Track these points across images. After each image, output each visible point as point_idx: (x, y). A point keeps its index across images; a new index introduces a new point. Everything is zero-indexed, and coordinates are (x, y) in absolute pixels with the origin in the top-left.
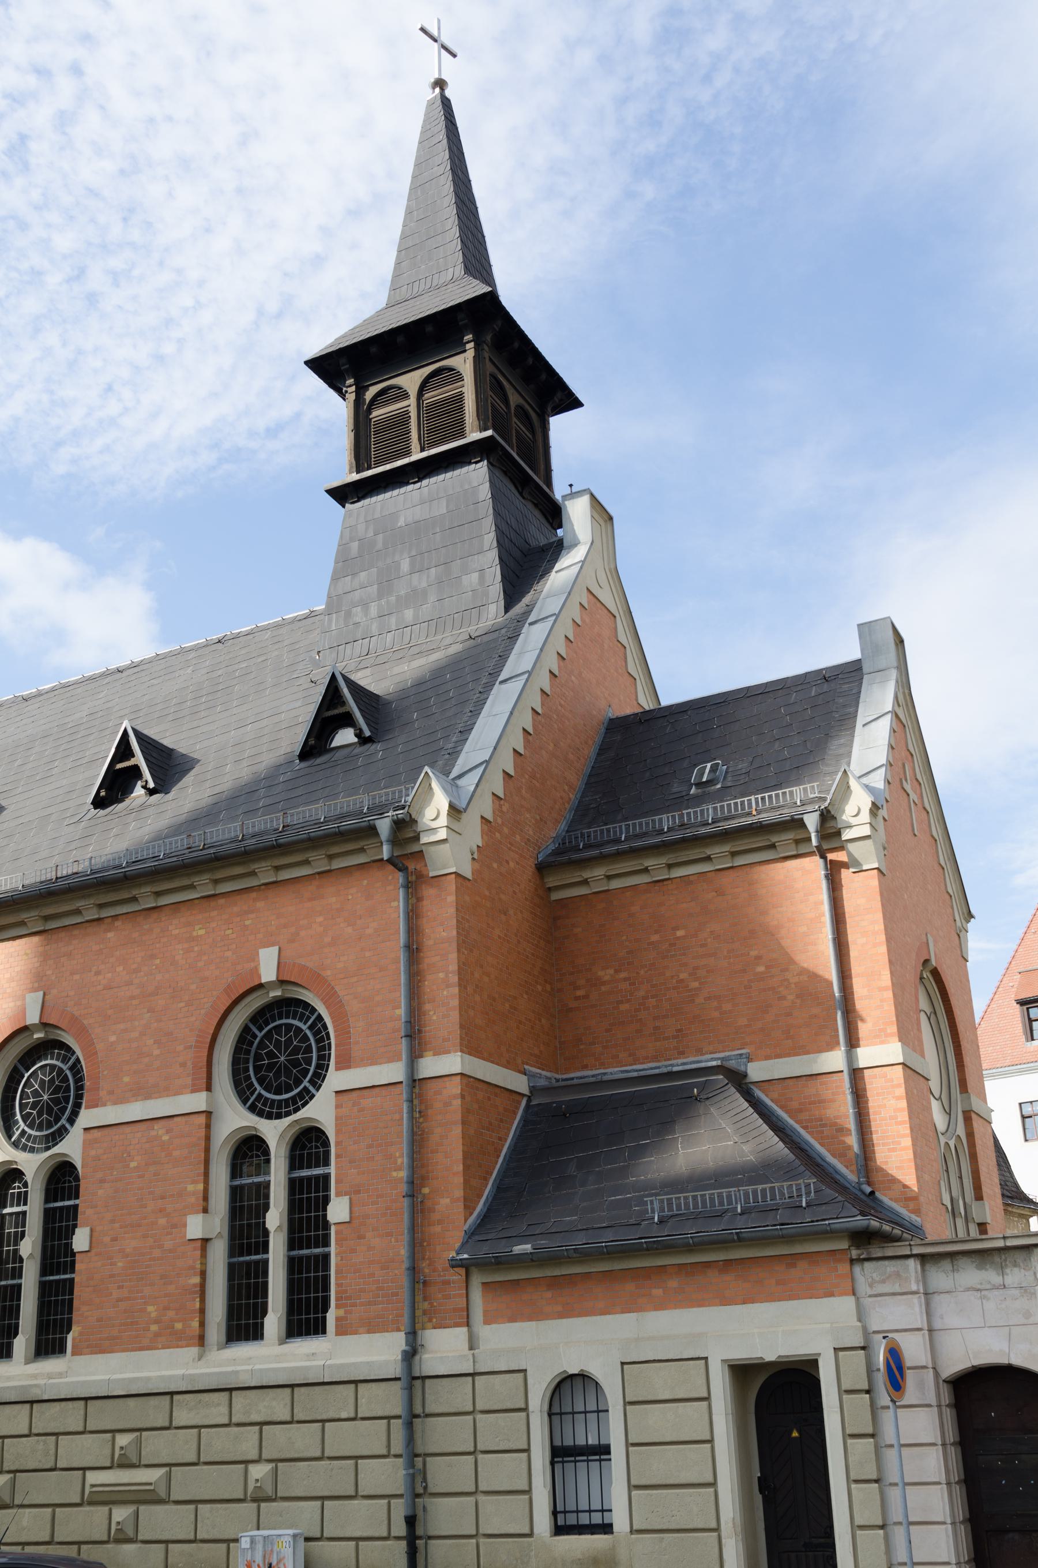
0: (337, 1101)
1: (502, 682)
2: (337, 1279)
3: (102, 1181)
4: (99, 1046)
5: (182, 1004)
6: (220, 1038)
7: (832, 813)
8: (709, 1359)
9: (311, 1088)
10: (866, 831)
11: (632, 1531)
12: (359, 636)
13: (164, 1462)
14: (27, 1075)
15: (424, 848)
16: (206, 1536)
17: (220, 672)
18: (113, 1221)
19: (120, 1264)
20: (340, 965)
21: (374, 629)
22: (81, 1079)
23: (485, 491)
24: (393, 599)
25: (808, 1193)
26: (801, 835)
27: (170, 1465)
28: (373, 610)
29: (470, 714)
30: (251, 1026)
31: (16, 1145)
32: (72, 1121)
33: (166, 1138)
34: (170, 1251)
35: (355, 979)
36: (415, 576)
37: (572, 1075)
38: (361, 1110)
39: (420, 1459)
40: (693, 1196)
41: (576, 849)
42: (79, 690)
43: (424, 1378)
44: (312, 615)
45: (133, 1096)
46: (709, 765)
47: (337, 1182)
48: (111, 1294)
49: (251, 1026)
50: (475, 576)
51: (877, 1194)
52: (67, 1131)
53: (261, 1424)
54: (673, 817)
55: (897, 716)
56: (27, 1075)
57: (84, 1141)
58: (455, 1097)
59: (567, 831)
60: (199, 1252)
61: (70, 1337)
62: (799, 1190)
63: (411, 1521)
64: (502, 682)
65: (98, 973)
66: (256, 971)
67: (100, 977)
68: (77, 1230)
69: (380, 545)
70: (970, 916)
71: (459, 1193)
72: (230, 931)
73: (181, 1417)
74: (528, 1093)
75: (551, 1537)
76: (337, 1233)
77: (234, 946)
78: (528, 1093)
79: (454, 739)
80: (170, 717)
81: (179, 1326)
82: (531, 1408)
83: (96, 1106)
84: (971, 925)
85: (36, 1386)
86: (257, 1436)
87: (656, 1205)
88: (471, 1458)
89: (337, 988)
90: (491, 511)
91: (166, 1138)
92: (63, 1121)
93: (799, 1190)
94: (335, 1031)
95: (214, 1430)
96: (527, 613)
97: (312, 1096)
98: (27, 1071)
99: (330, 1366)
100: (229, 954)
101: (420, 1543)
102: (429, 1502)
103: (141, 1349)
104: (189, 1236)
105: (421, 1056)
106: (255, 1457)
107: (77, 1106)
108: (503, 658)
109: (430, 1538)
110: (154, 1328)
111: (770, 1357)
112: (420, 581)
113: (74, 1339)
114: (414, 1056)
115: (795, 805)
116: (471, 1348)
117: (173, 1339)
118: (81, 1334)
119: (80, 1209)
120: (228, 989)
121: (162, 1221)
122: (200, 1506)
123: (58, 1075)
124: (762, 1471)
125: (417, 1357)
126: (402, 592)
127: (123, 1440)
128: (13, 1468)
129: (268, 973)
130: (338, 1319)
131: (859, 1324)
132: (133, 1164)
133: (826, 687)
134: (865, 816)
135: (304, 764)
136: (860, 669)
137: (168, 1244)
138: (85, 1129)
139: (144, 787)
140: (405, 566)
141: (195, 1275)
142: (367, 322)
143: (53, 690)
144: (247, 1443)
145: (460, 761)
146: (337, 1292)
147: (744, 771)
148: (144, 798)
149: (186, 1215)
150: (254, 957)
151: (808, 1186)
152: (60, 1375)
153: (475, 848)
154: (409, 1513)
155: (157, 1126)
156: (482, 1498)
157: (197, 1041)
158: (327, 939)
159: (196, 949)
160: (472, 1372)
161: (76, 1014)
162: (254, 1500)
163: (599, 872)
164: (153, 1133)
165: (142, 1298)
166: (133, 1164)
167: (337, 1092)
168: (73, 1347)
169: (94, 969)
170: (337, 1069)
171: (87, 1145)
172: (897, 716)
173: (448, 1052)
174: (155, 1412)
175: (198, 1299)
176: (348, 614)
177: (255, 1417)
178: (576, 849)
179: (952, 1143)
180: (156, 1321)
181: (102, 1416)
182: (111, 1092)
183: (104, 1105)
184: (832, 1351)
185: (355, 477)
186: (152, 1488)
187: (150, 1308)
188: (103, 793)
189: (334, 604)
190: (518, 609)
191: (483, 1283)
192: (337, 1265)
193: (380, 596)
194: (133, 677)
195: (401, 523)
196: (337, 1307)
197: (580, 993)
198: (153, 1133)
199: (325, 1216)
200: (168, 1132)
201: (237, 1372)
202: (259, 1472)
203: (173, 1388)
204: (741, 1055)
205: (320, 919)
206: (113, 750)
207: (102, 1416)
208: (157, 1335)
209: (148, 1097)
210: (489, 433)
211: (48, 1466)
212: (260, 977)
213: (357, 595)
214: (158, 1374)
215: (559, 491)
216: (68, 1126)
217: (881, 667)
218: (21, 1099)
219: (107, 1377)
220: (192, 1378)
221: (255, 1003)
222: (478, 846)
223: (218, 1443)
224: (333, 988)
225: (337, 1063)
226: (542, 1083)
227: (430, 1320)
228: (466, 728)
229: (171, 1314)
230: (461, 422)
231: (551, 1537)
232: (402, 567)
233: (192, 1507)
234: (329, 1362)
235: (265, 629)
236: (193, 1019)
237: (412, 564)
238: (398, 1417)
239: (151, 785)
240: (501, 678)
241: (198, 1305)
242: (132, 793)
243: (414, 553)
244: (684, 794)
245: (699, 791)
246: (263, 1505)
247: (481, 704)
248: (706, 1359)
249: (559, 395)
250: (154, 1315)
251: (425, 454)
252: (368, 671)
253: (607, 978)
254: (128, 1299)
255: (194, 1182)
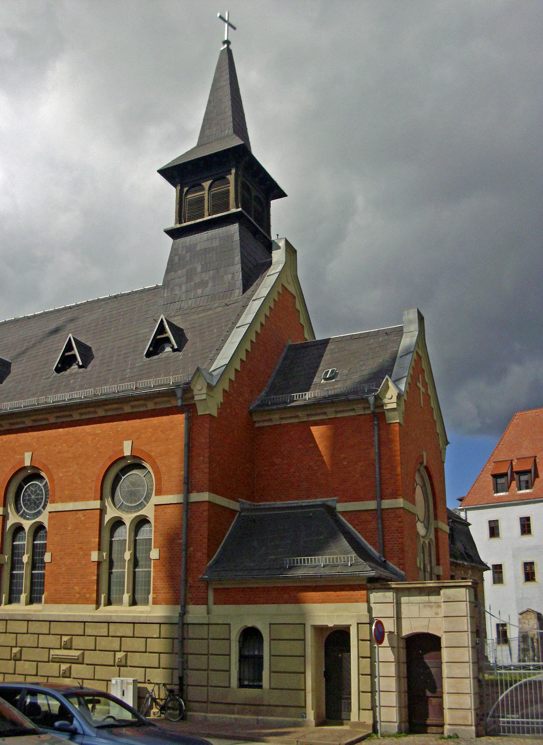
0: (155, 509)
1: (237, 328)
2: (153, 582)
3: (56, 534)
4: (55, 477)
5: (90, 462)
6: (107, 478)
7: (381, 397)
8: (306, 625)
9: (145, 502)
10: (394, 406)
11: (270, 688)
12: (177, 300)
13: (82, 648)
14: (25, 487)
15: (196, 402)
16: (98, 678)
17: (115, 312)
18: (60, 551)
19: (64, 569)
20: (158, 451)
21: (184, 298)
22: (48, 491)
23: (237, 237)
24: (193, 283)
25: (351, 560)
26: (367, 405)
27: (84, 650)
28: (184, 289)
29: (222, 341)
30: (120, 473)
31: (22, 516)
32: (44, 507)
33: (83, 518)
34: (85, 565)
35: (164, 457)
36: (203, 274)
37: (260, 503)
38: (165, 513)
39: (185, 655)
40: (307, 559)
41: (268, 405)
42: (52, 316)
43: (188, 624)
44: (157, 287)
45: (69, 500)
46: (330, 370)
47: (154, 542)
48: (60, 581)
49: (120, 473)
50: (230, 276)
51: (387, 562)
52: (42, 512)
53: (121, 637)
54: (311, 393)
55: (417, 353)
56: (25, 487)
57: (49, 518)
58: (205, 511)
59: (265, 396)
60: (96, 567)
61: (43, 596)
62: (348, 558)
63: (181, 679)
64: (237, 328)
65: (55, 446)
66: (122, 451)
67: (56, 448)
68: (46, 554)
69: (188, 259)
70: (447, 443)
71: (205, 551)
72: (111, 432)
73: (88, 631)
74: (240, 511)
75: (238, 688)
76: (154, 563)
77: (113, 439)
78: (240, 511)
79: (213, 353)
80: (91, 332)
81: (88, 595)
82: (232, 639)
83: (54, 503)
84: (448, 447)
85: (30, 614)
86: (119, 641)
87: (288, 561)
88: (206, 656)
89: (157, 461)
90: (239, 246)
91: (83, 518)
92: (40, 508)
93: (348, 558)
94: (155, 479)
95: (102, 638)
96: (252, 295)
97: (146, 506)
98: (26, 485)
99: (150, 616)
100: (111, 442)
101: (185, 687)
102: (189, 672)
103: (72, 603)
104: (92, 560)
105: (191, 492)
106: (119, 650)
107: (46, 502)
108: (239, 316)
109: (189, 685)
110: (78, 595)
111: (331, 625)
112: (206, 277)
113: (45, 598)
114: (188, 492)
115: (363, 392)
116: (208, 613)
117: (84, 600)
118: (48, 595)
119: (47, 545)
120: (110, 458)
121: (81, 553)
122: (96, 666)
123: (39, 488)
124: (325, 669)
125: (185, 616)
126: (197, 281)
127: (65, 639)
128: (21, 646)
129: (127, 452)
130: (153, 598)
131: (368, 614)
132: (69, 528)
133: (386, 337)
134: (394, 399)
135: (148, 359)
136: (402, 330)
137: (84, 562)
138: (49, 512)
139: (78, 364)
140: (199, 269)
141: (95, 575)
142: (169, 164)
143: (41, 314)
144: (115, 644)
145: (215, 364)
146: (153, 587)
147: (346, 374)
148: (77, 369)
149: (91, 551)
150: (121, 445)
151: (351, 557)
152: (39, 611)
153: (220, 403)
154: (181, 675)
155: (79, 513)
156: (211, 673)
157: (96, 479)
158: (153, 439)
159: (97, 439)
160: (208, 623)
161: (46, 463)
162: (118, 666)
163: (277, 416)
164: (77, 516)
165: (73, 583)
166: (69, 528)
167: (155, 505)
168: (45, 600)
169: (54, 444)
170: (156, 495)
171: (50, 519)
172: (417, 353)
173: (203, 491)
174: (78, 629)
175: (96, 586)
176: (172, 289)
177: (119, 634)
178: (268, 405)
179: (427, 542)
180: (79, 593)
181: (56, 629)
182: (60, 498)
183: (57, 502)
184: (356, 624)
185: (178, 226)
186: (77, 658)
187: (76, 588)
188: (60, 366)
189: (167, 283)
190: (249, 292)
191: (214, 589)
192: (153, 576)
193: (187, 283)
194: (76, 312)
195: (198, 248)
196: (153, 593)
197: (266, 468)
198: (77, 516)
199: (149, 556)
200: (84, 516)
201: (111, 616)
202: (119, 655)
203: (85, 620)
204: (334, 500)
205: (150, 430)
206: (64, 347)
207: (56, 629)
208: (79, 598)
209: (76, 500)
210: (240, 209)
211: (35, 646)
212: (124, 453)
213: (177, 281)
214: (79, 614)
215: (273, 237)
216: (42, 510)
217: (412, 330)
218: (23, 498)
219: (59, 613)
220: (94, 617)
221: (121, 465)
222: (221, 403)
223: (103, 643)
224: (155, 460)
225: (155, 493)
226: (247, 506)
227: (192, 601)
228: (220, 348)
229: (85, 591)
230: (228, 203)
231: (238, 688)
232: (197, 269)
233: (93, 666)
234: (149, 615)
235: (136, 292)
236: (95, 469)
237: (202, 268)
238: (177, 638)
239: (81, 364)
240: (238, 325)
241: (95, 588)
242: (72, 366)
243: (203, 263)
244: (318, 382)
245: (325, 381)
246: (121, 668)
247: (227, 337)
248: (304, 624)
249: (276, 191)
250: (78, 590)
251: (210, 217)
252: (179, 317)
253: (278, 463)
254: (67, 583)
255: (94, 538)
